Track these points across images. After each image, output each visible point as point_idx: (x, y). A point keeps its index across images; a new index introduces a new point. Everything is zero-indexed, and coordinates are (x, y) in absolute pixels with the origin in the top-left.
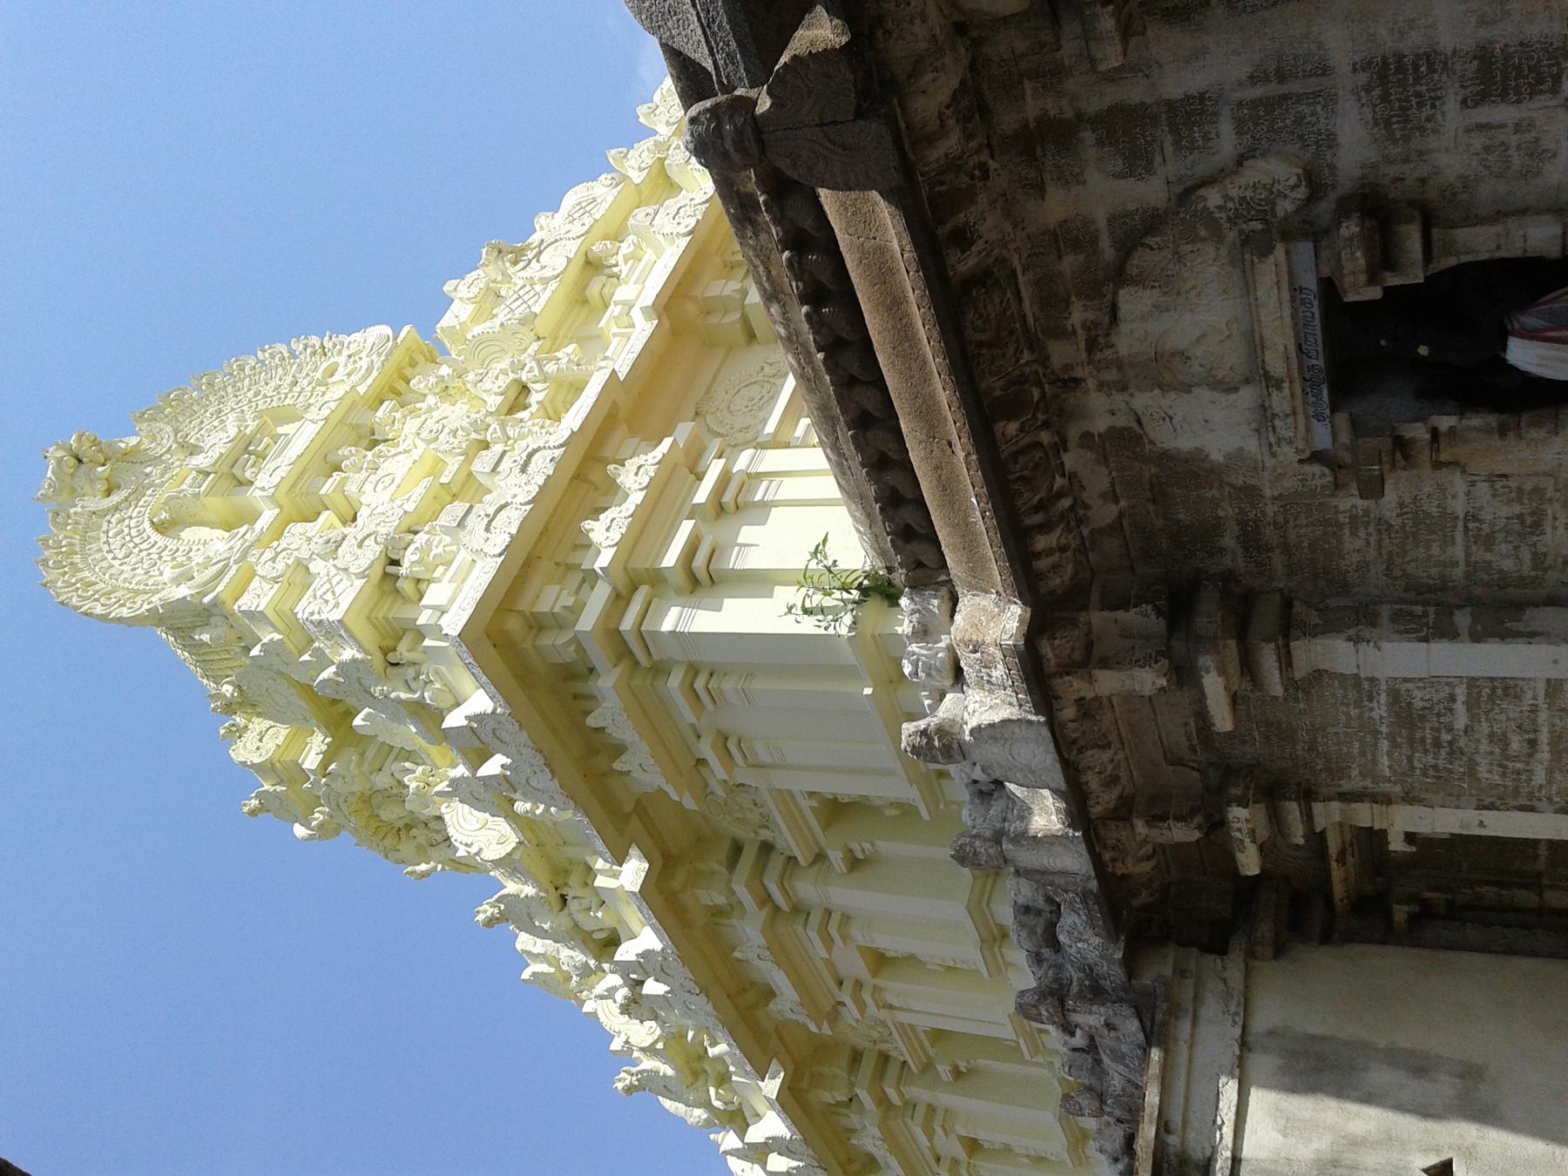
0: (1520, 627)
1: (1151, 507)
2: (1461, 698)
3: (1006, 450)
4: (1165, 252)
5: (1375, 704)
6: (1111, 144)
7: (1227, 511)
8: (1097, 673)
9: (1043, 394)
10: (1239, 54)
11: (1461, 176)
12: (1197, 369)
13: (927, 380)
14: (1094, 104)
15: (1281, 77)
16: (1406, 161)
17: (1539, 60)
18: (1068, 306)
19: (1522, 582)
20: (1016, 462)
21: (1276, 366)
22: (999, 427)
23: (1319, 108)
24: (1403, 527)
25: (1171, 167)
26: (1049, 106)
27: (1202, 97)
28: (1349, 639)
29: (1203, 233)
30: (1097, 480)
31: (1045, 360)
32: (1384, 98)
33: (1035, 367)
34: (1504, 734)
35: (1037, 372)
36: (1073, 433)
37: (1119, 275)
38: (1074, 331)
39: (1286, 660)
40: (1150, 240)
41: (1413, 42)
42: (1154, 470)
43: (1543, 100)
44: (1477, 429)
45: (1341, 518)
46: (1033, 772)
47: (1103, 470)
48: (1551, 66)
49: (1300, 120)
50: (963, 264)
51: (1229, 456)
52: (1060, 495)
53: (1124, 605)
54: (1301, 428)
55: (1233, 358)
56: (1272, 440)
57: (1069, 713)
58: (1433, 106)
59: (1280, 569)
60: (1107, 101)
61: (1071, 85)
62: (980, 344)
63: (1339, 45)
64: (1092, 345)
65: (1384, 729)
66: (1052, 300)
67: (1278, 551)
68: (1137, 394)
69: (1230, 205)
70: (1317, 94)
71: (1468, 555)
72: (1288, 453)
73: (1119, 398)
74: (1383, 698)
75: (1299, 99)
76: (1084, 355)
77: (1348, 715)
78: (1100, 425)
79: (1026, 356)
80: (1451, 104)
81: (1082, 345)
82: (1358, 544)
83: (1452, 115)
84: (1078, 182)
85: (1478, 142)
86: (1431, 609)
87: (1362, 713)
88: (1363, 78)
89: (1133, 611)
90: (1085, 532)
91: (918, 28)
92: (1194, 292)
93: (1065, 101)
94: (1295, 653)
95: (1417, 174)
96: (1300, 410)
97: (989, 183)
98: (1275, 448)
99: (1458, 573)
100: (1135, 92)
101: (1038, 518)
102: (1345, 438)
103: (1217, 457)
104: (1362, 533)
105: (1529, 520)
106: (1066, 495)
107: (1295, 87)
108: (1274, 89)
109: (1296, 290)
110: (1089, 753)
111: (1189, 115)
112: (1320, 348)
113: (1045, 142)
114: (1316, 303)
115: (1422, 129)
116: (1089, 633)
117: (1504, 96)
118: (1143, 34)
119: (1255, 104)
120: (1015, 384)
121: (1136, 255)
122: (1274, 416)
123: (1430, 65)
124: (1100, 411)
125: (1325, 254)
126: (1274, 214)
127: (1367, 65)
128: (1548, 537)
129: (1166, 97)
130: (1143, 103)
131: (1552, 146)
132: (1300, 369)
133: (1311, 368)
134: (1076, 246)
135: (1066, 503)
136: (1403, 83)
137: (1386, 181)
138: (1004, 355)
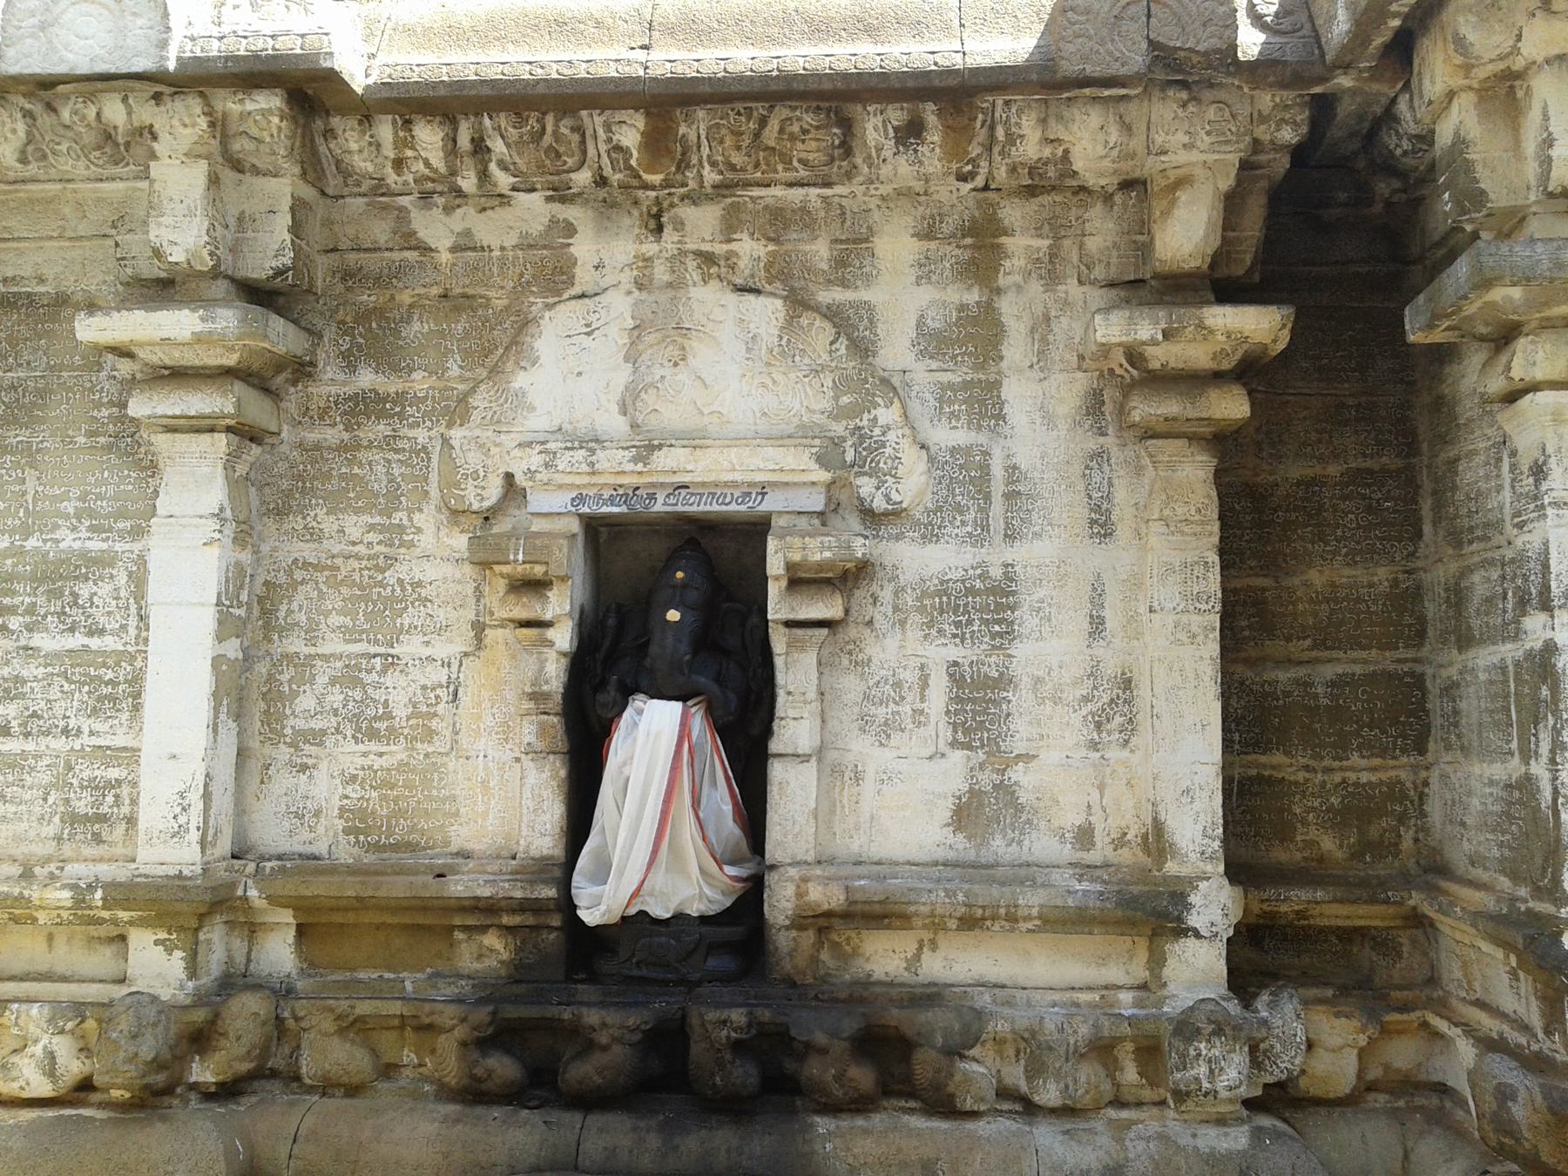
0: (223, 717)
1: (435, 291)
2: (95, 643)
3: (595, 121)
4: (825, 356)
5: (84, 535)
6: (959, 318)
7: (420, 382)
8: (200, 170)
9: (646, 186)
10: (1042, 458)
11: (870, 660)
12: (658, 372)
13: (749, 40)
14: (1008, 307)
15: (1010, 496)
16: (896, 609)
17: (988, 730)
18: (770, 239)
19: (273, 719)
20: (573, 129)
21: (664, 460)
22: (639, 121)
23: (969, 529)
24: (381, 584)
25: (924, 376)
26: (1015, 261)
27: (1001, 417)
28: (222, 510)
29: (845, 400)
30: (497, 230)
31: (693, 199)
32: (971, 591)
33: (692, 184)
34: (23, 696)
35: (684, 185)
36: (572, 213)
37: (798, 303)
38: (729, 241)
39: (202, 426)
40: (842, 346)
41: (1026, 619)
42: (500, 304)
43: (946, 734)
44: (541, 669)
45: (399, 517)
46: (43, 27)
47: (511, 240)
48: (981, 739)
49: (960, 509)
50: (875, 128)
51: (521, 394)
52: (484, 175)
53: (296, 229)
54: (568, 479)
55: (668, 413)
56: (551, 446)
57: (114, 111)
58: (955, 636)
59: (312, 436)
60: (1008, 320)
61: (1035, 287)
62: (763, 122)
63: (1031, 555)
64: (708, 259)
65: (32, 543)
66: (778, 222)
67: (346, 436)
68: (630, 300)
69: (877, 431)
70: (985, 528)
71: (326, 658)
72: (522, 464)
73: (627, 277)
74: (96, 545)
75: (984, 511)
76: (691, 246)
77: (64, 497)
78: (583, 248)
79: (710, 176)
80: (954, 652)
81: (706, 247)
82: (354, 533)
83: (942, 653)
84: (919, 278)
85: (910, 676)
86: (241, 612)
87: (67, 517)
88: (996, 572)
89: (288, 237)
90: (404, 201)
91: (1182, 138)
92: (769, 382)
93: (1018, 278)
94: (206, 438)
95: (878, 617)
96: (595, 479)
97: (952, 179)
98: (539, 448)
99: (296, 645)
100: (1016, 349)
101: (464, 141)
102: (538, 526)
103: (521, 381)
104: (372, 537)
105: (382, 726)
106: (480, 187)
107: (997, 507)
108: (998, 487)
109: (763, 490)
110: (21, 127)
111: (984, 403)
112: (680, 508)
113: (980, 248)
114: (743, 508)
115: (930, 625)
116: (256, 171)
117: (958, 699)
118: (1079, 368)
119: (985, 468)
120: (683, 154)
121: (827, 325)
122: (593, 451)
123: (1000, 635)
124: (605, 251)
125: (803, 522)
126: (858, 474)
127: (1009, 577)
128: (350, 746)
129: (1005, 382)
130: (1001, 358)
131: (893, 743)
132: (653, 485)
133: (652, 497)
134: (840, 263)
135: (468, 182)
136: (985, 609)
137: (875, 587)
138: (739, 148)
